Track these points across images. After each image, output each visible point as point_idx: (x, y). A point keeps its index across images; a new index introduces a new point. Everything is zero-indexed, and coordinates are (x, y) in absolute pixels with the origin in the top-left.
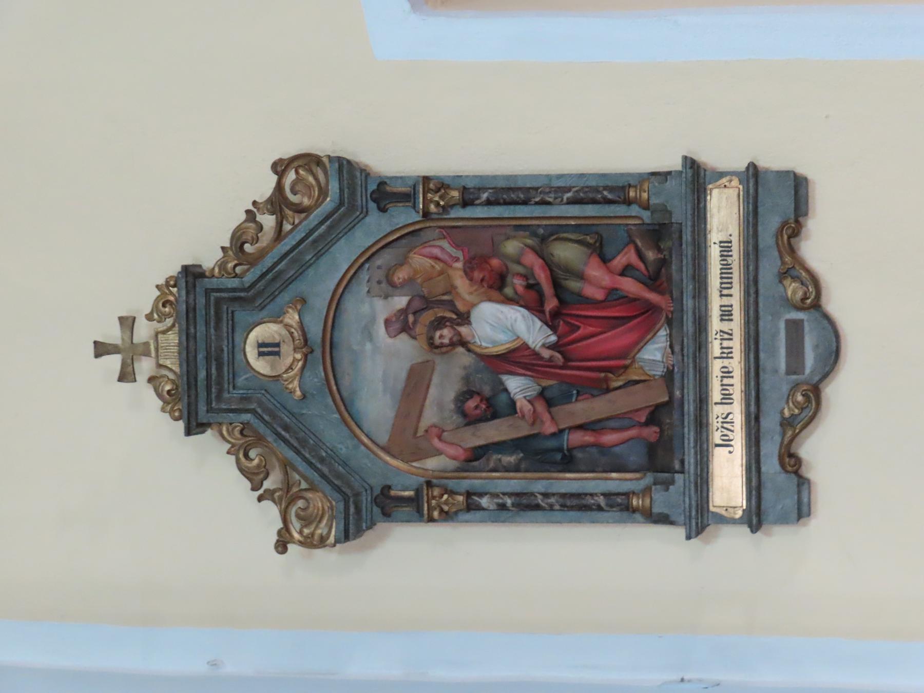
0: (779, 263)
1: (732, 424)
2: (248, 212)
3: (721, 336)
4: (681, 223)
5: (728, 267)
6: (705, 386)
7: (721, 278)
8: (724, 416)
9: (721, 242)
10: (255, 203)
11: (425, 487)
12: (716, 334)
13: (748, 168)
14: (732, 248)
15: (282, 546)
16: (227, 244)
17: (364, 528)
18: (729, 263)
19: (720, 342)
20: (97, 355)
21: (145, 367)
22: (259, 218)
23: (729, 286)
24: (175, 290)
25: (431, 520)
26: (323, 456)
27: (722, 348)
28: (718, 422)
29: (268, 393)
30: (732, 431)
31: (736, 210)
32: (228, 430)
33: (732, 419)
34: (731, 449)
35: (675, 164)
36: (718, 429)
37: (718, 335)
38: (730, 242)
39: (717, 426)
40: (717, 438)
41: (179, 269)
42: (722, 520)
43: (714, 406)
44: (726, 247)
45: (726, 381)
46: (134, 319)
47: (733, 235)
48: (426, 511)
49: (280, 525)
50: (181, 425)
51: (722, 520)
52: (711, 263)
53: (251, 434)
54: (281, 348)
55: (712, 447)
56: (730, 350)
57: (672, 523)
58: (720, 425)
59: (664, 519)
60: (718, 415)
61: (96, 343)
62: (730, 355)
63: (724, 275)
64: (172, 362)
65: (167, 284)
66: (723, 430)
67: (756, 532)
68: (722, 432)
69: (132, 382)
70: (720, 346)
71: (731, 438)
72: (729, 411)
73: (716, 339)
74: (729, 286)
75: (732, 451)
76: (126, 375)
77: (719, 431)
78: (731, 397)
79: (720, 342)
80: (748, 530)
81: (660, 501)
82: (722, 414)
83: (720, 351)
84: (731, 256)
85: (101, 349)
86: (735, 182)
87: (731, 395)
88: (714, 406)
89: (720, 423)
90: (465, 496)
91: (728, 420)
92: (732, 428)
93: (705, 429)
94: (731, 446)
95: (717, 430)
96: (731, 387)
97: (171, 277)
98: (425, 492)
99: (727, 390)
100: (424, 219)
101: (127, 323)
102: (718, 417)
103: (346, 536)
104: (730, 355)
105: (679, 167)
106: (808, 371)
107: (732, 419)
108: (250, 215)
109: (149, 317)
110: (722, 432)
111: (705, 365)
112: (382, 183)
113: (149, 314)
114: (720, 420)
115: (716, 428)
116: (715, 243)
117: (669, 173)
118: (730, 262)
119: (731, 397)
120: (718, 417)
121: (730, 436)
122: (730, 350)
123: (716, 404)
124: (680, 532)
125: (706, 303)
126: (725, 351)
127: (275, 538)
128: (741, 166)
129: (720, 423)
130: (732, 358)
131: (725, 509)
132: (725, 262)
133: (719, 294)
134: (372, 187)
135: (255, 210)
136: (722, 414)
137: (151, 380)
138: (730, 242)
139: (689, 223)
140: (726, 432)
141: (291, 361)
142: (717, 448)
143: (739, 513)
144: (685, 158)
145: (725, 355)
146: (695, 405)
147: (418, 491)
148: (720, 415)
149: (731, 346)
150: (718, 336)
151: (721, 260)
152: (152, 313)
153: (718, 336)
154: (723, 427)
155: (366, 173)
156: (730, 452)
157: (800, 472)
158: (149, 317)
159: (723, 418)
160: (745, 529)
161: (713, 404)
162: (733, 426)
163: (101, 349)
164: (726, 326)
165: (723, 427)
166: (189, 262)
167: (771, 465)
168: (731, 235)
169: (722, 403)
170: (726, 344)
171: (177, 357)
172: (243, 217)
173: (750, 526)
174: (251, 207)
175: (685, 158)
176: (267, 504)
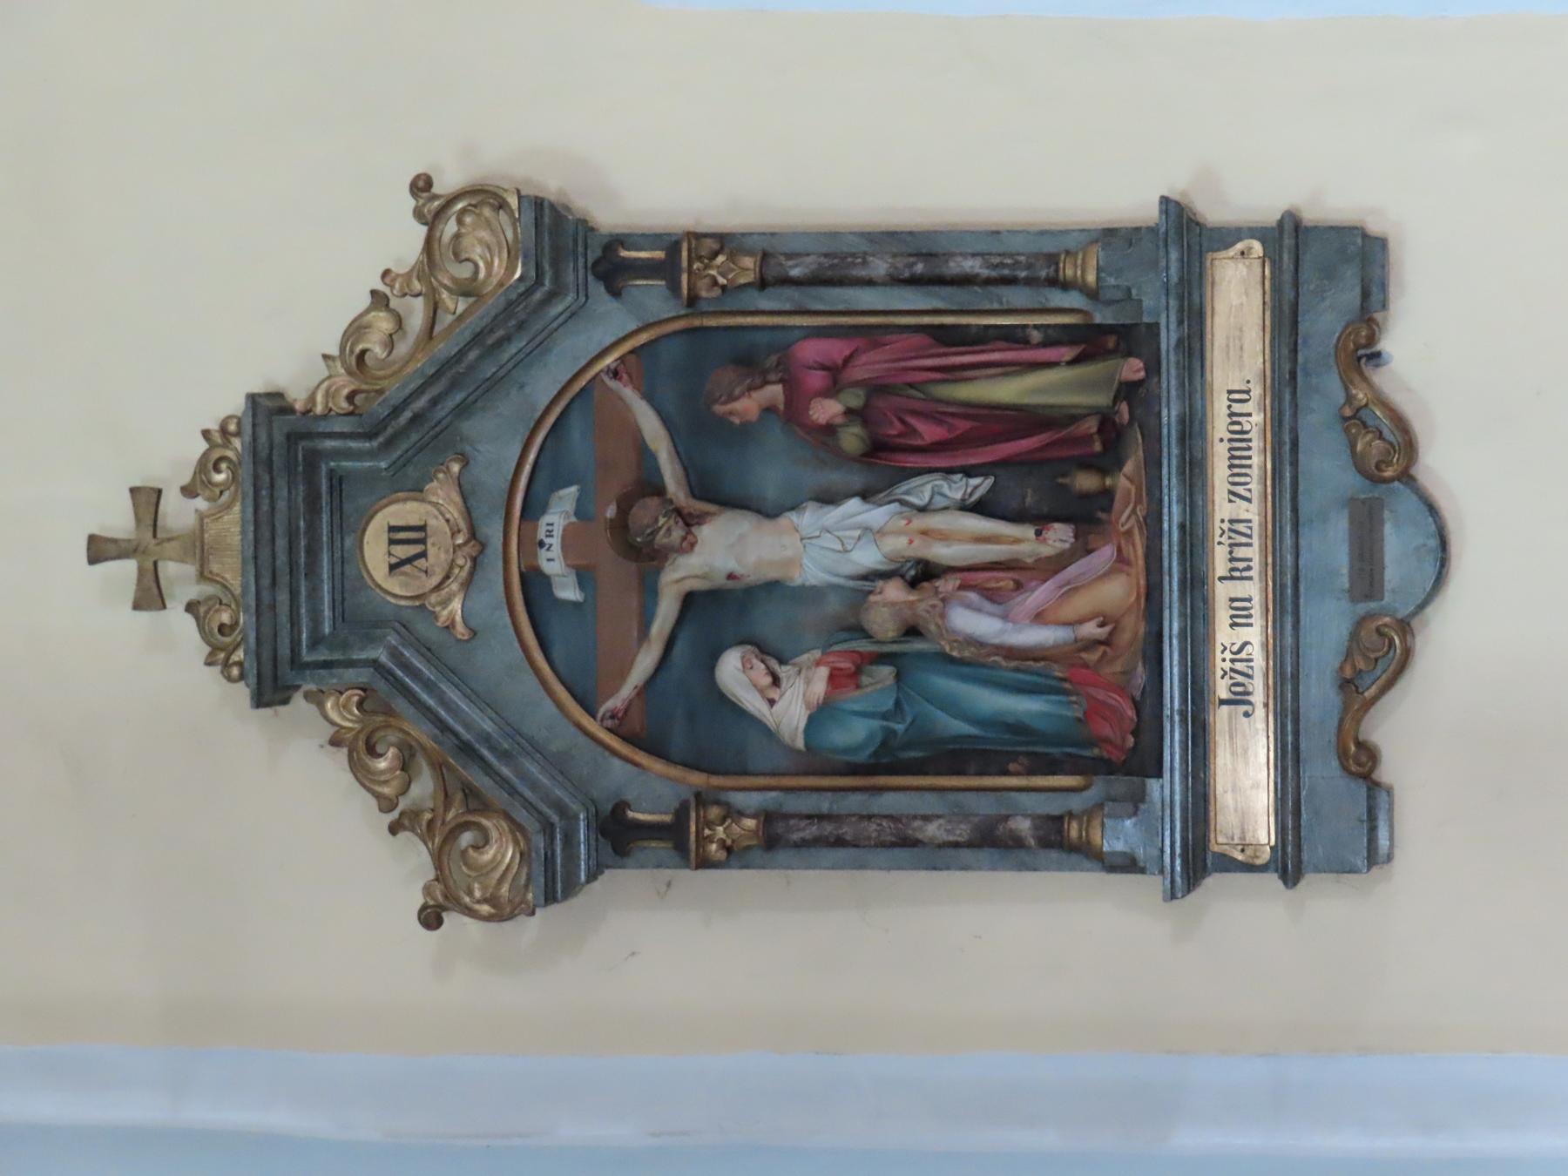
0: (1340, 398)
1: (1250, 525)
2: (374, 293)
5: (1245, 436)
6: (1199, 368)
8: (1235, 648)
11: (693, 805)
12: (1221, 536)
13: (1281, 223)
15: (431, 918)
16: (334, 351)
17: (583, 877)
18: (1244, 429)
19: (1229, 549)
20: (93, 559)
21: (180, 577)
23: (1245, 396)
24: (237, 443)
25: (704, 863)
26: (505, 749)
27: (1232, 560)
28: (1224, 660)
32: (337, 704)
36: (1225, 673)
37: (1225, 536)
38: (1248, 392)
39: (1222, 529)
40: (1222, 690)
41: (235, 404)
42: (1227, 864)
43: (1218, 583)
44: (1238, 396)
45: (1237, 408)
46: (159, 492)
48: (693, 846)
50: (242, 692)
51: (1227, 864)
52: (1213, 501)
57: (1142, 871)
58: (1226, 526)
60: (1226, 645)
61: (137, 606)
62: (1245, 574)
63: (1237, 462)
64: (231, 570)
66: (1233, 675)
67: (1295, 884)
68: (1230, 538)
69: (160, 609)
70: (1229, 557)
72: (1245, 639)
73: (1220, 543)
74: (1245, 396)
75: (1250, 712)
76: (150, 596)
77: (1227, 677)
78: (1246, 698)
79: (1229, 549)
80: (1280, 884)
81: (1120, 835)
82: (1233, 644)
83: (1230, 565)
85: (99, 549)
86: (1257, 247)
88: (1218, 583)
89: (1226, 441)
90: (762, 819)
91: (1243, 655)
92: (1250, 672)
94: (1249, 703)
95: (1222, 678)
96: (1246, 418)
97: (230, 417)
98: (693, 815)
99: (1239, 423)
100: (690, 311)
101: (147, 499)
102: (1225, 648)
103: (550, 898)
104: (1245, 574)
107: (1250, 654)
108: (379, 300)
109: (188, 491)
110: (1231, 678)
111: (1200, 456)
112: (618, 241)
113: (379, 801)
114: (1228, 655)
115: (1221, 531)
118: (1247, 427)
119: (1246, 698)
123: (1223, 702)
124: (1150, 886)
126: (1241, 565)
127: (418, 900)
128: (1270, 217)
129: (1224, 656)
131: (1240, 847)
132: (1237, 428)
136: (1233, 644)
137: (191, 607)
138: (1248, 392)
140: (1240, 679)
142: (1225, 708)
143: (1266, 855)
144: (1165, 201)
145: (1237, 574)
146: (1183, 624)
147: (681, 813)
149: (1249, 556)
151: (1231, 475)
152: (378, 796)
155: (585, 228)
156: (1247, 715)
157: (1375, 776)
158: (188, 491)
161: (1216, 544)
166: (258, 387)
167: (1322, 770)
168: (1248, 382)
169: (1232, 578)
170: (1237, 408)
172: (366, 301)
175: (1165, 201)
176: (404, 836)
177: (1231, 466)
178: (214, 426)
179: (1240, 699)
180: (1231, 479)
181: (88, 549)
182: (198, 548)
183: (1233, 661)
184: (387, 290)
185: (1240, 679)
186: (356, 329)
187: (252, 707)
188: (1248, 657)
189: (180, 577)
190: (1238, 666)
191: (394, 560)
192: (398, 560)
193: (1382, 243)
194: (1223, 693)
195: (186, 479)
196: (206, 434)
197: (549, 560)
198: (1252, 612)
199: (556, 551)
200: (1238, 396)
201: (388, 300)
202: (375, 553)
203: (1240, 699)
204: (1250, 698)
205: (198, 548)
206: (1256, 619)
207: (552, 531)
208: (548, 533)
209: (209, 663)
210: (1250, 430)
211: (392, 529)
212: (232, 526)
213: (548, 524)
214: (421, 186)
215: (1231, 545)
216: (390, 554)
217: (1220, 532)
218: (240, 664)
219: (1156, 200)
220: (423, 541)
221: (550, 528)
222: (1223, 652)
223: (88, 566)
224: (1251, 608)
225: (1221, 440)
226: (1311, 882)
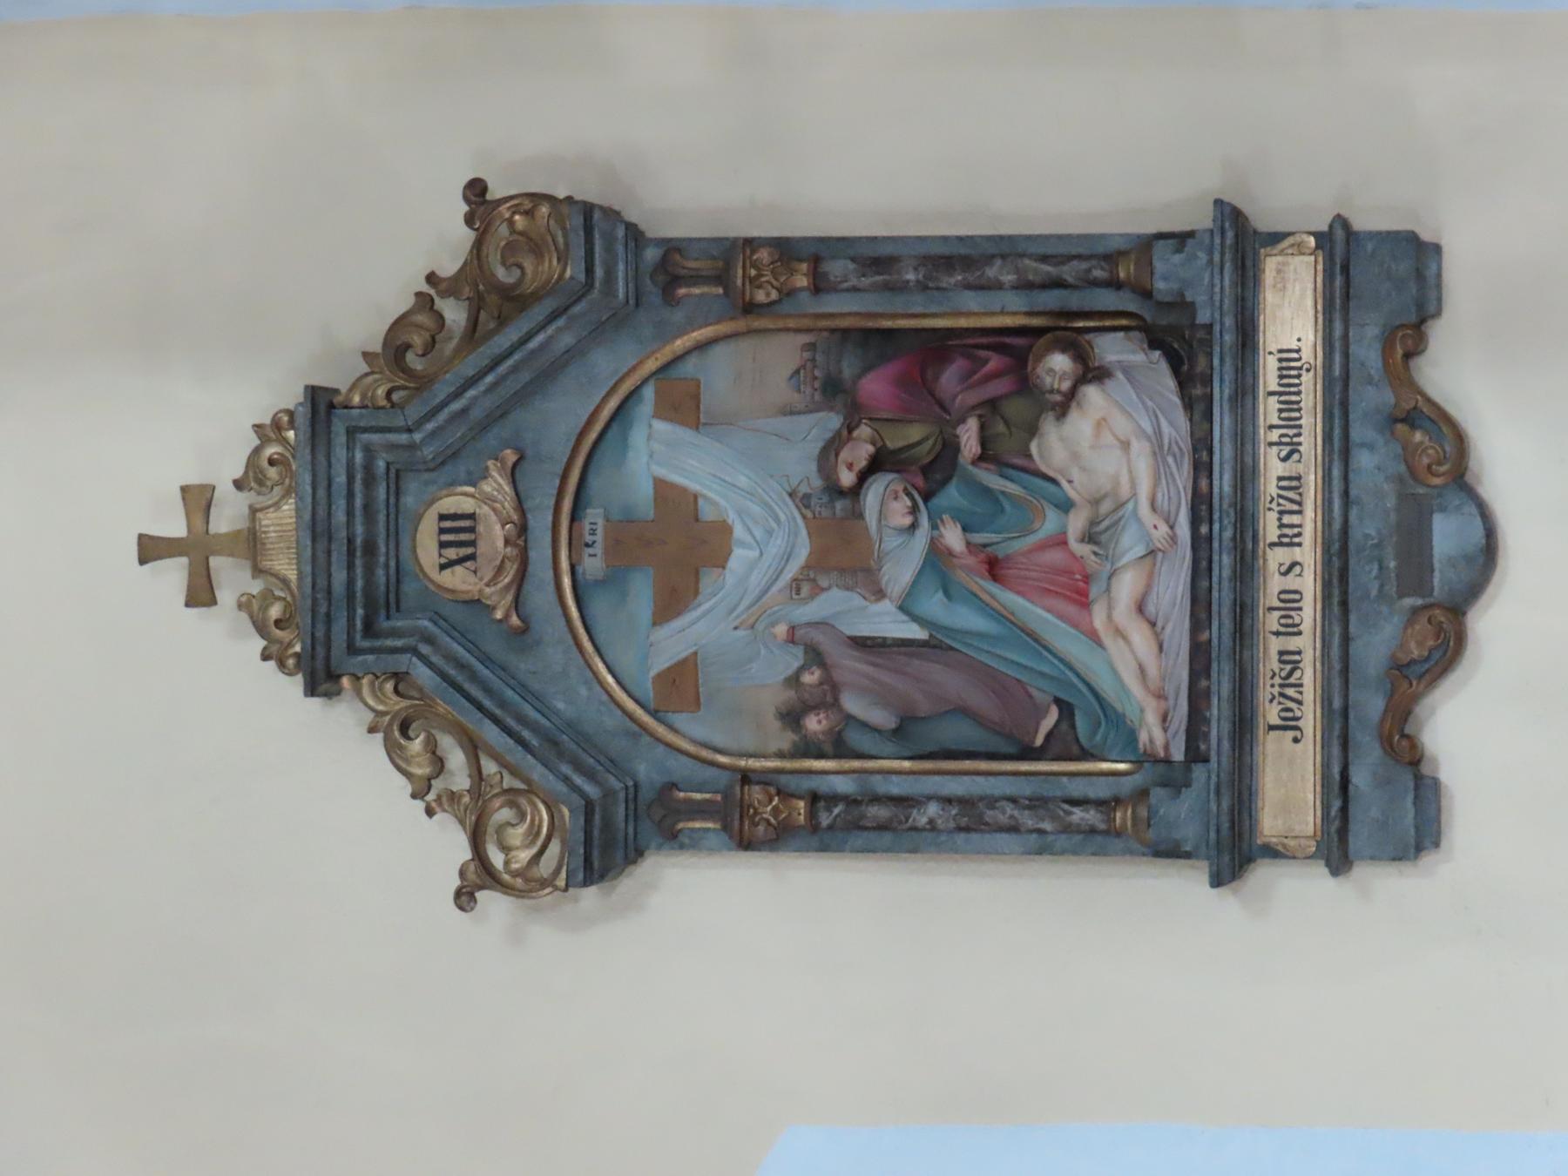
1: (1301, 689)
2: (419, 295)
3: (1279, 505)
4: (1211, 325)
7: (1280, 360)
8: (1283, 674)
9: (1280, 351)
10: (431, 278)
14: (1301, 628)
15: (464, 898)
16: (377, 347)
21: (232, 579)
22: (440, 304)
27: (1281, 526)
28: (1272, 686)
29: (456, 629)
30: (1300, 703)
31: (1310, 286)
33: (1300, 679)
34: (1298, 734)
35: (1202, 219)
39: (1271, 694)
40: (1273, 715)
45: (1286, 519)
46: (214, 488)
47: (1303, 339)
49: (465, 854)
50: (296, 684)
51: (1273, 852)
53: (417, 695)
54: (478, 547)
55: (1264, 734)
56: (1296, 530)
57: (1187, 856)
58: (1276, 690)
59: (1169, 851)
62: (1296, 540)
63: (1285, 372)
65: (276, 425)
66: (1282, 700)
68: (1280, 703)
71: (1298, 714)
73: (1270, 509)
75: (1299, 737)
76: (201, 594)
77: (1275, 702)
80: (1326, 871)
82: (1281, 565)
83: (1278, 532)
84: (1300, 609)
85: (150, 549)
87: (1298, 719)
91: (1292, 680)
92: (1297, 498)
93: (1249, 736)
94: (1297, 728)
95: (1271, 701)
101: (198, 499)
102: (1274, 675)
104: (1296, 540)
105: (1207, 223)
106: (1436, 593)
114: (1277, 680)
115: (1270, 697)
116: (1270, 353)
117: (1190, 234)
119: (1298, 423)
120: (1274, 675)
121: (1296, 710)
122: (1296, 530)
123: (1272, 728)
125: (1254, 404)
130: (1299, 545)
133: (1277, 523)
134: (651, 255)
135: (432, 292)
139: (1229, 321)
141: (624, 795)
144: (1219, 203)
147: (727, 794)
148: (1277, 671)
150: (1274, 505)
151: (1283, 710)
153: (1274, 505)
154: (1282, 695)
156: (1296, 740)
158: (239, 485)
159: (1284, 679)
160: (1320, 870)
162: (1301, 693)
163: (150, 549)
164: (1291, 582)
165: (1282, 695)
169: (1281, 544)
171: (294, 561)
173: (1328, 864)
174: (425, 288)
175: (1219, 203)
177: (1281, 377)
178: (267, 420)
179: (1289, 724)
180: (1284, 714)
181: (146, 535)
182: (250, 544)
183: (1281, 686)
184: (432, 292)
185: (1291, 494)
186: (400, 323)
187: (306, 695)
188: (1298, 682)
189: (232, 579)
190: (1290, 692)
191: (443, 561)
192: (447, 561)
193: (1437, 844)
194: (1274, 719)
195: (239, 472)
196: (258, 428)
197: (590, 555)
198: (1302, 422)
199: (598, 549)
200: (1289, 540)
201: (432, 300)
202: (427, 547)
203: (1289, 724)
204: (1300, 723)
205: (250, 544)
206: (1305, 439)
207: (596, 530)
208: (591, 532)
209: (265, 657)
210: (1301, 623)
211: (442, 517)
212: (282, 518)
213: (591, 523)
214: (476, 190)
215: (1281, 513)
216: (440, 555)
217: (1269, 498)
218: (297, 655)
219: (1212, 201)
220: (472, 543)
221: (594, 527)
222: (1272, 678)
223: (139, 567)
224: (1300, 384)
225: (1272, 609)
226: (1362, 872)
